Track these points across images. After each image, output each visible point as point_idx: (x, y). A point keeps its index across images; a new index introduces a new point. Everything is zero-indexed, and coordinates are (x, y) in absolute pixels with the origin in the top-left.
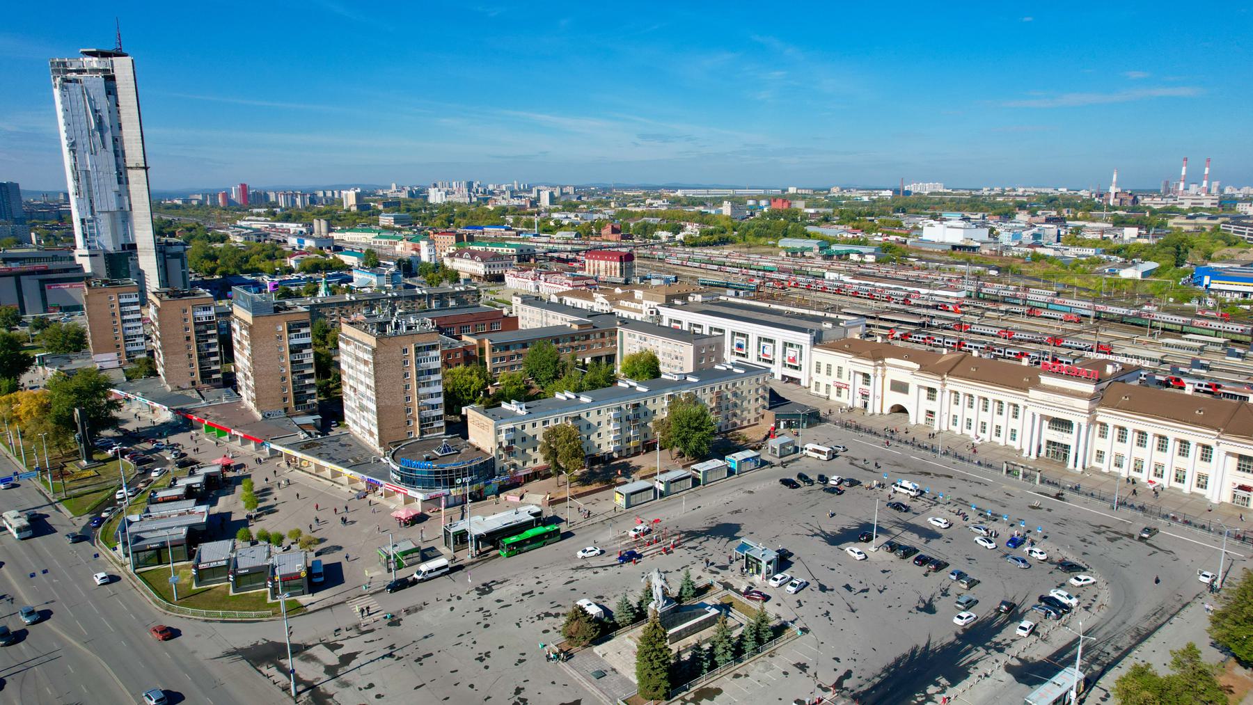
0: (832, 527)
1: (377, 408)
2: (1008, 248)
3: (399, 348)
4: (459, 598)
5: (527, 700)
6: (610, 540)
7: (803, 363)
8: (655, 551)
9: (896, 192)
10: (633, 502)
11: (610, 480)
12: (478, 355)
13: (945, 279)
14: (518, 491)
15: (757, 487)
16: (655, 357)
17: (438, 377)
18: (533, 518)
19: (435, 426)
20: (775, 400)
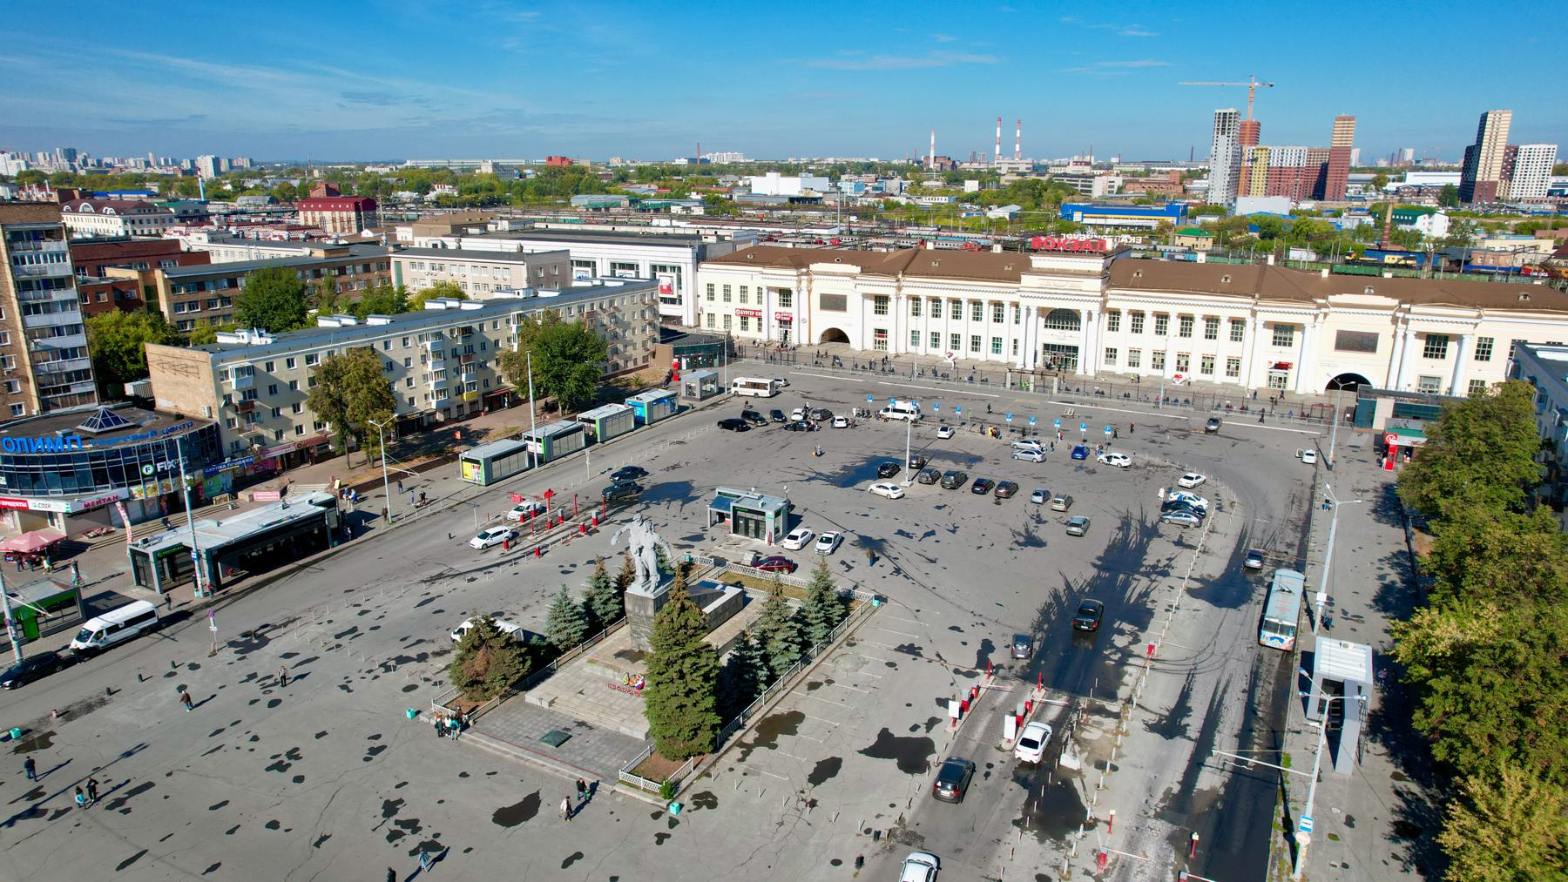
0: (830, 466)
4: (194, 667)
5: (417, 821)
7: (683, 293)
8: (569, 532)
9: (692, 160)
10: (496, 474)
11: (442, 451)
12: (143, 298)
14: (275, 482)
15: (688, 436)
19: (74, 391)
20: (668, 335)
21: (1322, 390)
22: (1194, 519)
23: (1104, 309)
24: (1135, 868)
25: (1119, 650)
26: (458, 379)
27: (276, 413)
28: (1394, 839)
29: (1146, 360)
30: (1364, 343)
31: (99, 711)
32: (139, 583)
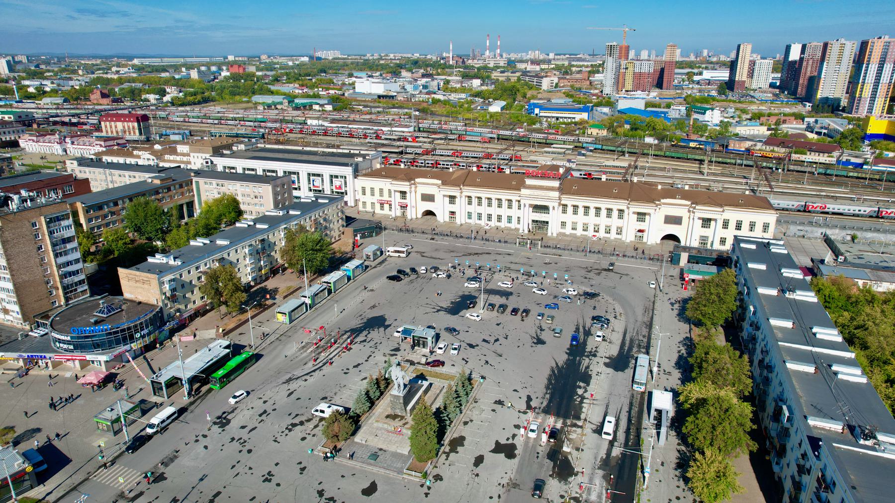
1: (15, 285)
2: (413, 96)
3: (26, 222)
6: (296, 352)
7: (348, 189)
9: (311, 58)
14: (187, 330)
16: (235, 199)
17: (74, 244)
18: (228, 351)
19: (79, 290)
20: (349, 220)
21: (659, 241)
23: (560, 204)
24: (593, 490)
25: (580, 396)
27: (184, 296)
28: (676, 469)
29: (580, 227)
30: (677, 221)
31: (176, 461)
32: (155, 394)
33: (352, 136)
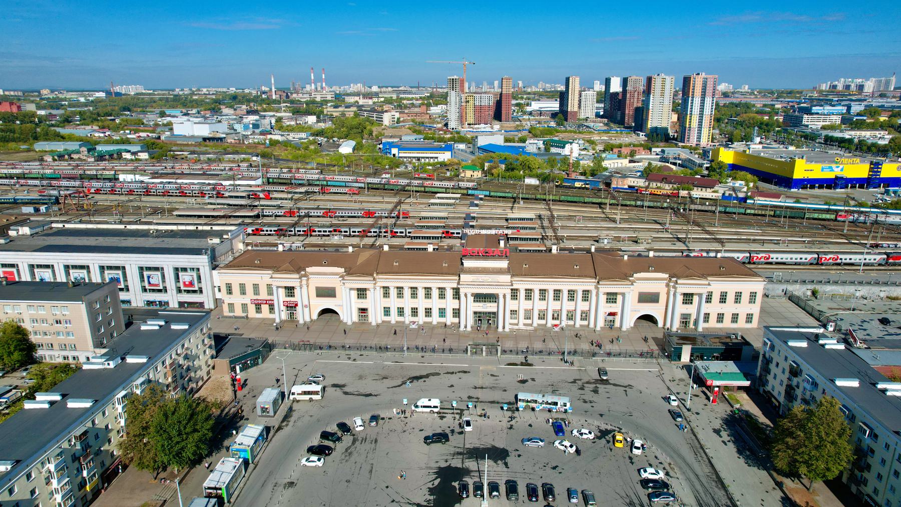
2: (246, 137)
7: (203, 285)
9: (108, 93)
13: (227, 168)
16: (19, 327)
22: (672, 499)
26: (80, 477)
30: (652, 298)
33: (183, 194)
